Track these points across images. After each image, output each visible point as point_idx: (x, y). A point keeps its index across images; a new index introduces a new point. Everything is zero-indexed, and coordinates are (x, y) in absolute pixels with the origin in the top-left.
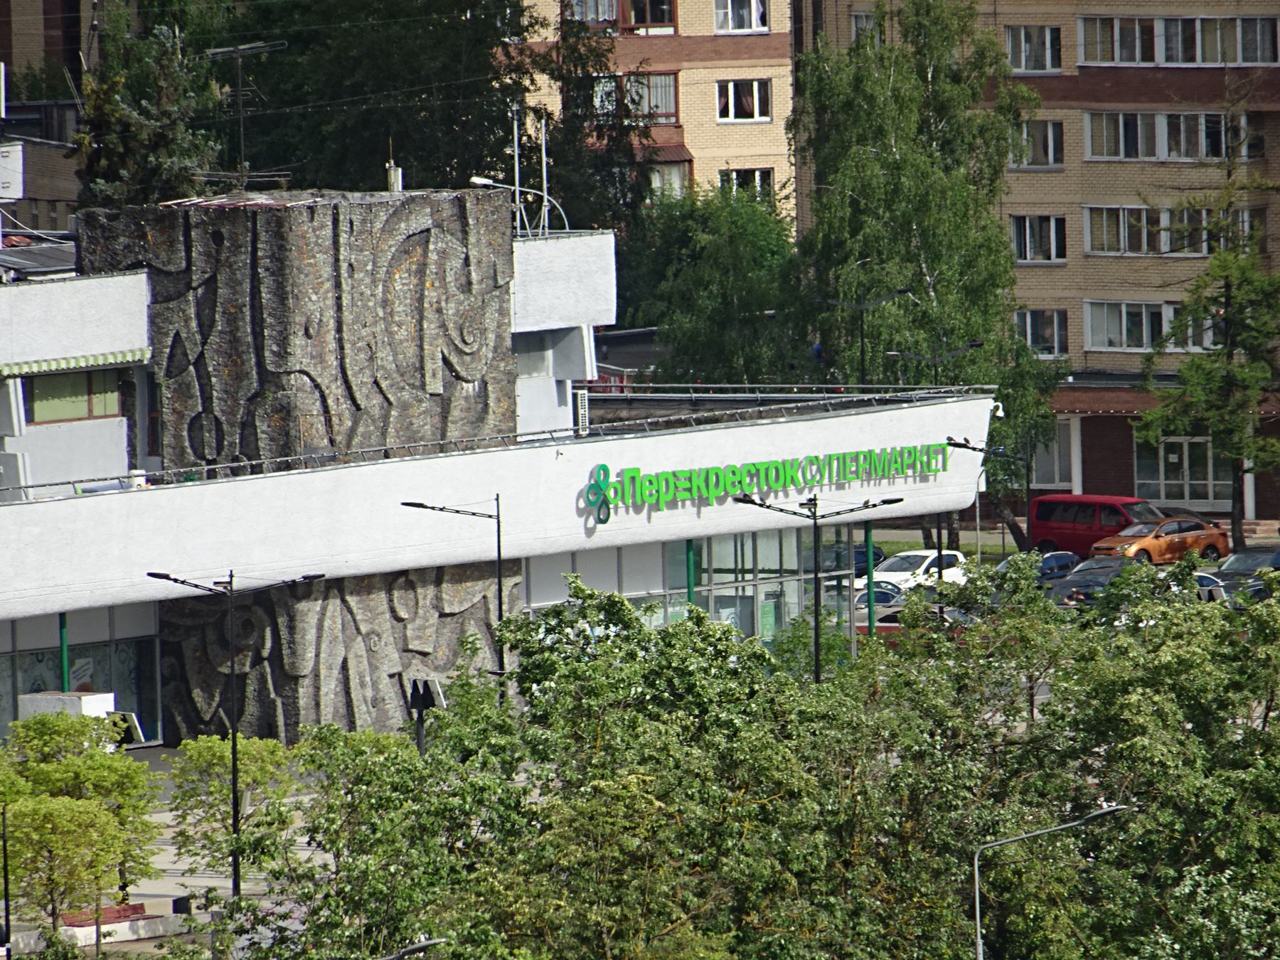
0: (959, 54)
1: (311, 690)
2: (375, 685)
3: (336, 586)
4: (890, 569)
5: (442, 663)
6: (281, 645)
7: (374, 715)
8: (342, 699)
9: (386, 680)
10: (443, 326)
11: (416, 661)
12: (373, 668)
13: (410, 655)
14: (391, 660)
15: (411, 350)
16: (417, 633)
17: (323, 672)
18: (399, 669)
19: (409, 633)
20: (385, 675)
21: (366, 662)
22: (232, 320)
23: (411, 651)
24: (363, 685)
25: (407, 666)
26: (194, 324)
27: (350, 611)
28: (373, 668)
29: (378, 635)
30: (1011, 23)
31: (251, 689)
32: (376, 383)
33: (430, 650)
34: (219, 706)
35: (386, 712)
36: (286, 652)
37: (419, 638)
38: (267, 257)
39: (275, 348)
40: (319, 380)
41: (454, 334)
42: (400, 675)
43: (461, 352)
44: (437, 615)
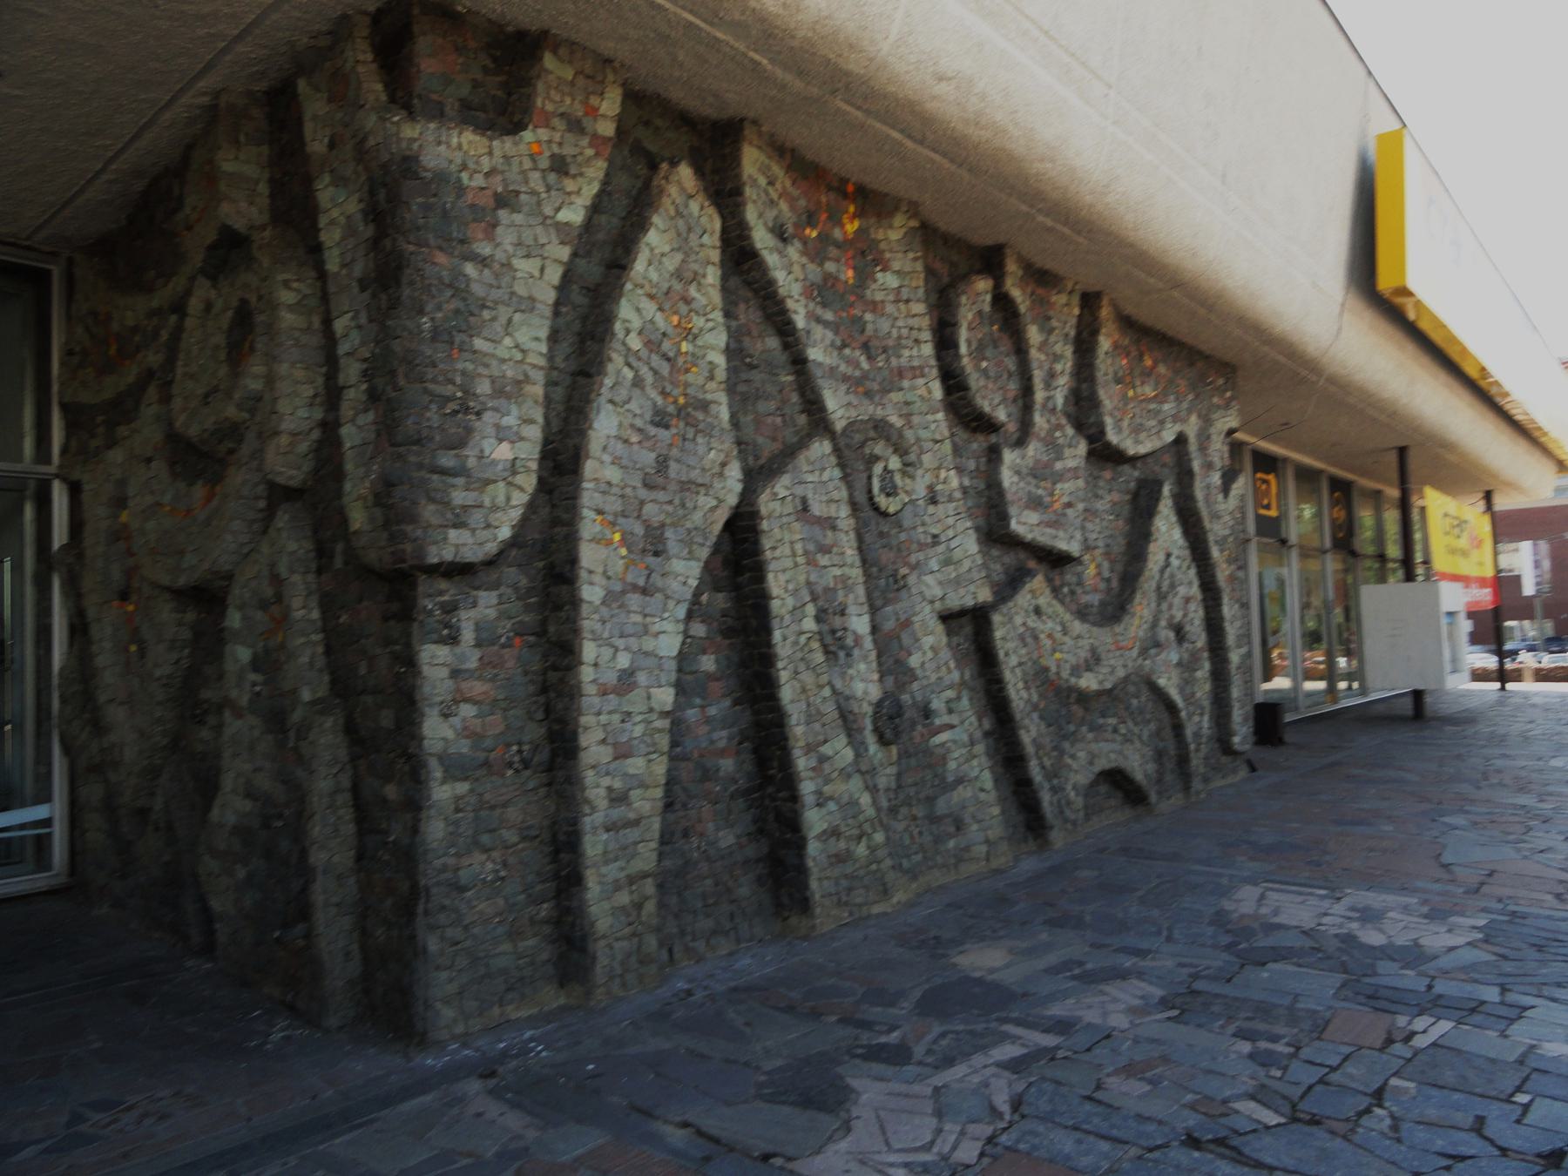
0: (696, 755)
2: (892, 664)
4: (1242, 498)
5: (1095, 599)
7: (885, 779)
8: (716, 723)
12: (884, 584)
14: (952, 567)
17: (600, 558)
18: (985, 595)
19: (1007, 478)
21: (851, 553)
24: (835, 645)
28: (884, 584)
29: (900, 450)
30: (810, 502)
33: (1074, 548)
35: (933, 761)
37: (1035, 503)
44: (1082, 448)
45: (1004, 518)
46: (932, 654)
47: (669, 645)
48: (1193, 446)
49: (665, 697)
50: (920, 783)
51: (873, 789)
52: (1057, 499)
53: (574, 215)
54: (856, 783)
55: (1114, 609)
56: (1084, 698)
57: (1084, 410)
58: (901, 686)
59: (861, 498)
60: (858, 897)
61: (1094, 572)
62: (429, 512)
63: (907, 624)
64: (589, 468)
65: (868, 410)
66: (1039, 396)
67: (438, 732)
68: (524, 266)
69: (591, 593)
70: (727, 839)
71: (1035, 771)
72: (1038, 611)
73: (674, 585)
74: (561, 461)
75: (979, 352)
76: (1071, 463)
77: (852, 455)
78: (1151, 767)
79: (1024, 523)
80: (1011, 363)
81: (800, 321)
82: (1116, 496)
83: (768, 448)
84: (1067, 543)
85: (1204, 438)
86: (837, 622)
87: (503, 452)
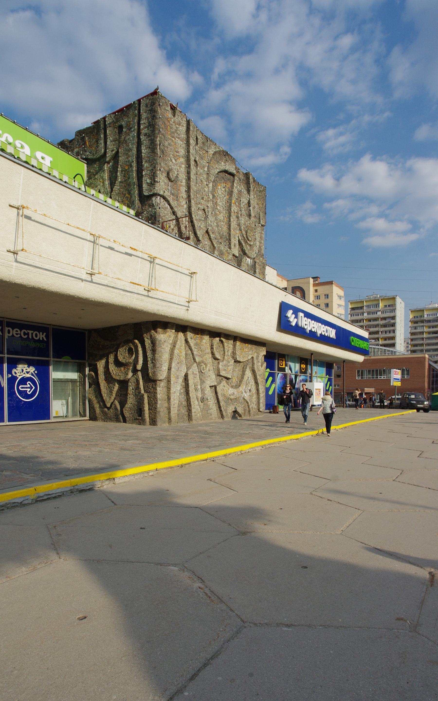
1: (165, 389)
2: (203, 390)
3: (182, 327)
5: (234, 385)
6: (147, 361)
7: (202, 407)
9: (209, 389)
10: (239, 225)
11: (224, 382)
13: (221, 378)
14: (212, 379)
15: (225, 228)
16: (224, 368)
17: (173, 379)
18: (216, 384)
19: (220, 366)
20: (208, 387)
22: (127, 174)
23: (221, 376)
24: (196, 390)
25: (220, 383)
26: (107, 183)
27: (191, 349)
28: (202, 382)
29: (205, 364)
31: (131, 388)
32: (207, 232)
33: (230, 377)
34: (115, 399)
36: (150, 365)
37: (225, 370)
38: (145, 128)
39: (148, 181)
40: (176, 209)
41: (244, 232)
42: (215, 387)
43: (246, 242)
44: (233, 361)
45: (219, 372)
46: (209, 393)
47: (179, 389)
48: (255, 359)
49: (178, 394)
50: (206, 410)
51: (200, 408)
52: (228, 368)
53: (171, 342)
54: (198, 407)
55: (238, 386)
56: (231, 400)
57: (234, 353)
58: (204, 395)
59: (200, 371)
60: (198, 420)
61: (234, 380)
62: (159, 374)
63: (205, 387)
64: (172, 369)
65: (201, 359)
66: (226, 354)
67: (159, 396)
68: (166, 348)
69: (172, 383)
70: (183, 412)
71: (222, 409)
72: (224, 386)
73: (179, 382)
74: (169, 369)
75: (217, 349)
76: (231, 364)
77: (199, 364)
78: (243, 412)
79: (223, 373)
80: (222, 349)
81: (193, 349)
82: (239, 368)
83: (189, 365)
84: (229, 376)
85: (258, 357)
86: (196, 387)
87: (165, 368)
